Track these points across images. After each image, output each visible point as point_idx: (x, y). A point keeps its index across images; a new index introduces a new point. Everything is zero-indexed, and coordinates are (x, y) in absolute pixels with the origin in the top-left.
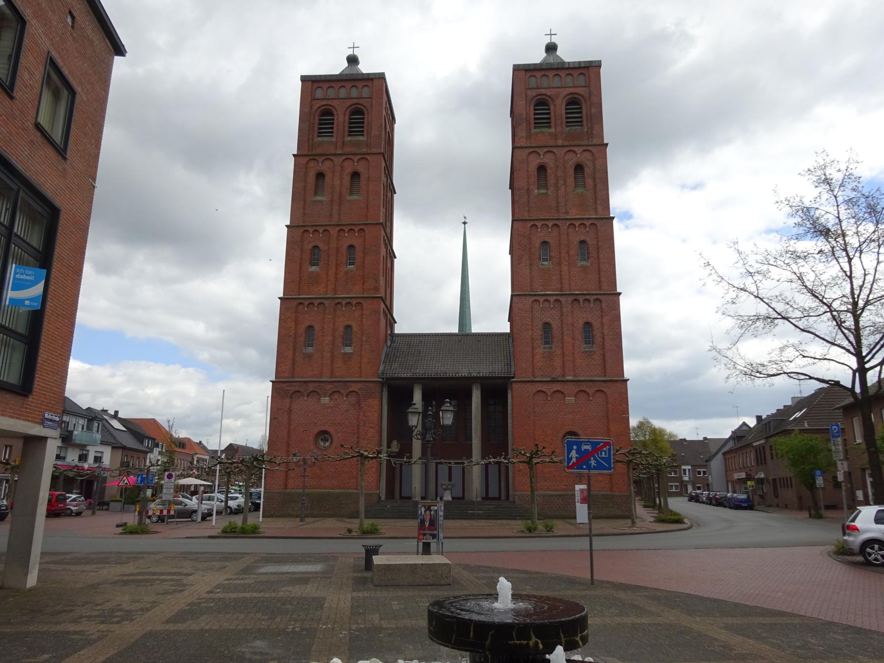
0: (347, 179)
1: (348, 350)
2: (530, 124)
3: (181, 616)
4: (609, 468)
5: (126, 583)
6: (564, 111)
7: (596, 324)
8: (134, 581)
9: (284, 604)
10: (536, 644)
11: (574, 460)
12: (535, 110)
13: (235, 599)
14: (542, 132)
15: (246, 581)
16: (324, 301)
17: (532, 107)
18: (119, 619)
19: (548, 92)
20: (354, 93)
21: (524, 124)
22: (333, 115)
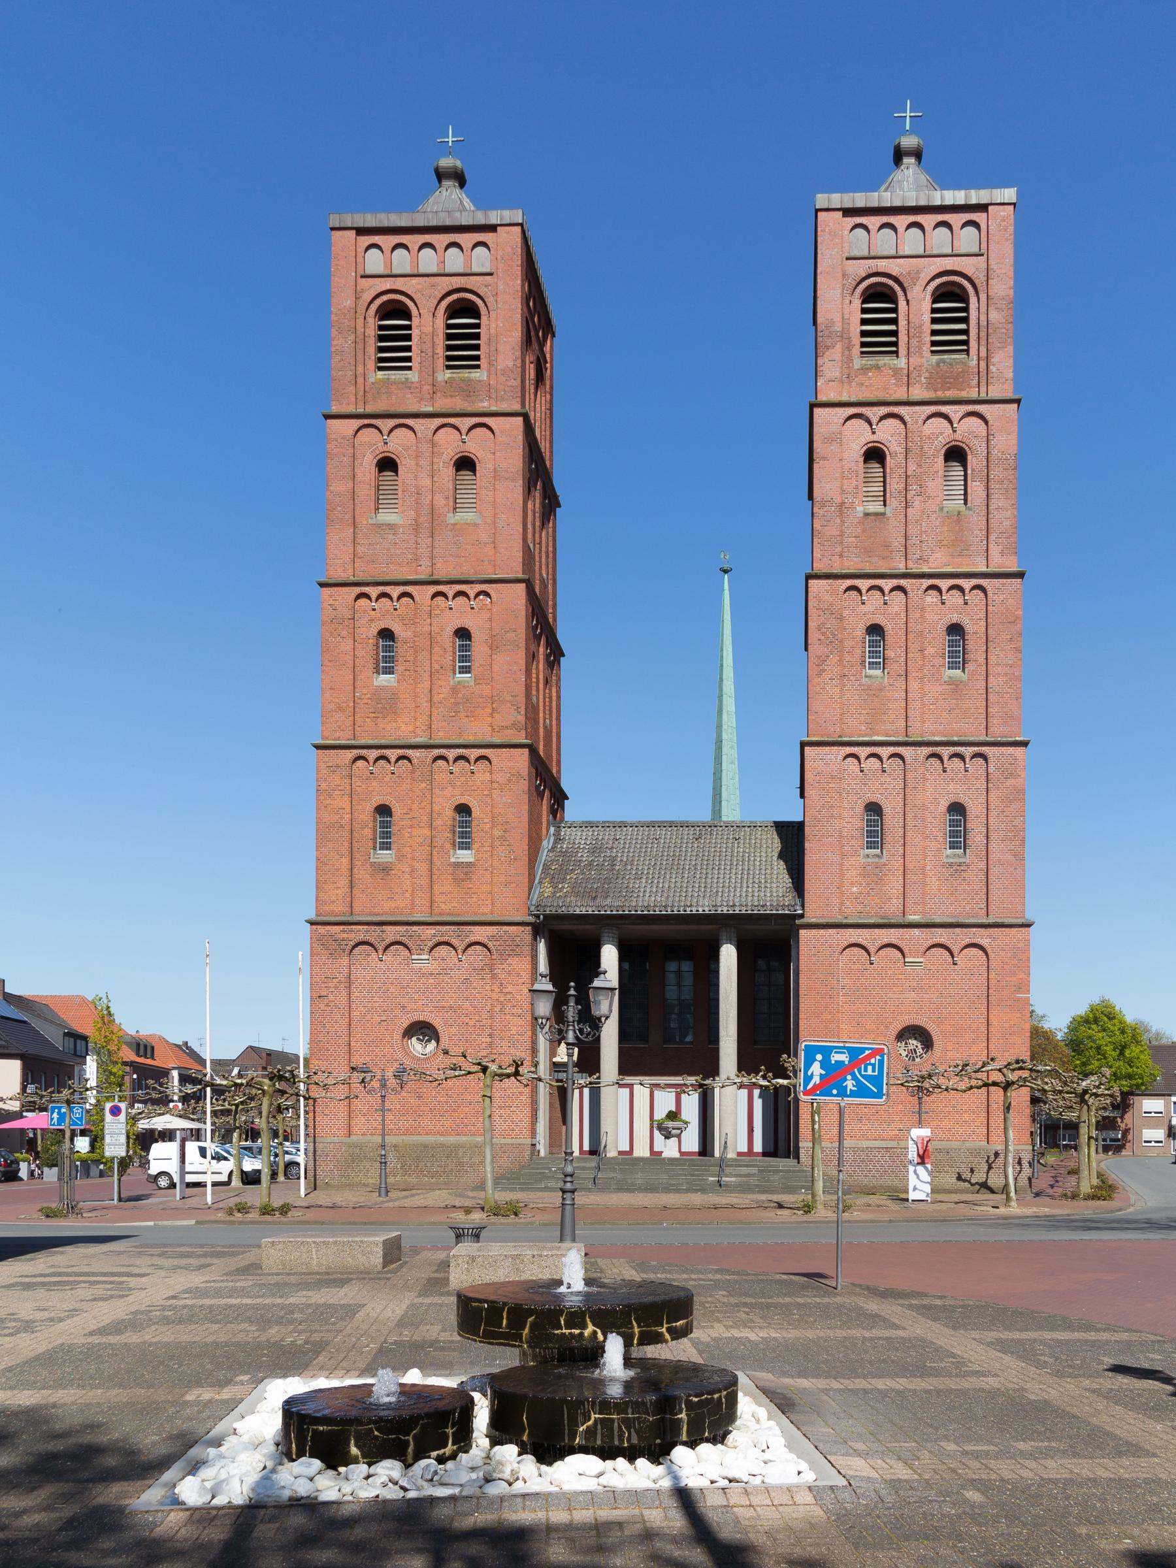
0: (447, 472)
1: (465, 856)
2: (849, 348)
3: (117, 1327)
4: (879, 1095)
5: (28, 1287)
6: (927, 316)
7: (974, 808)
8: (43, 1284)
9: (292, 1312)
10: (595, 1333)
11: (816, 1080)
12: (864, 311)
13: (211, 1306)
14: (877, 367)
15: (238, 1284)
16: (409, 752)
17: (857, 303)
18: (11, 1331)
19: (893, 267)
20: (455, 260)
21: (839, 346)
22: (407, 315)
